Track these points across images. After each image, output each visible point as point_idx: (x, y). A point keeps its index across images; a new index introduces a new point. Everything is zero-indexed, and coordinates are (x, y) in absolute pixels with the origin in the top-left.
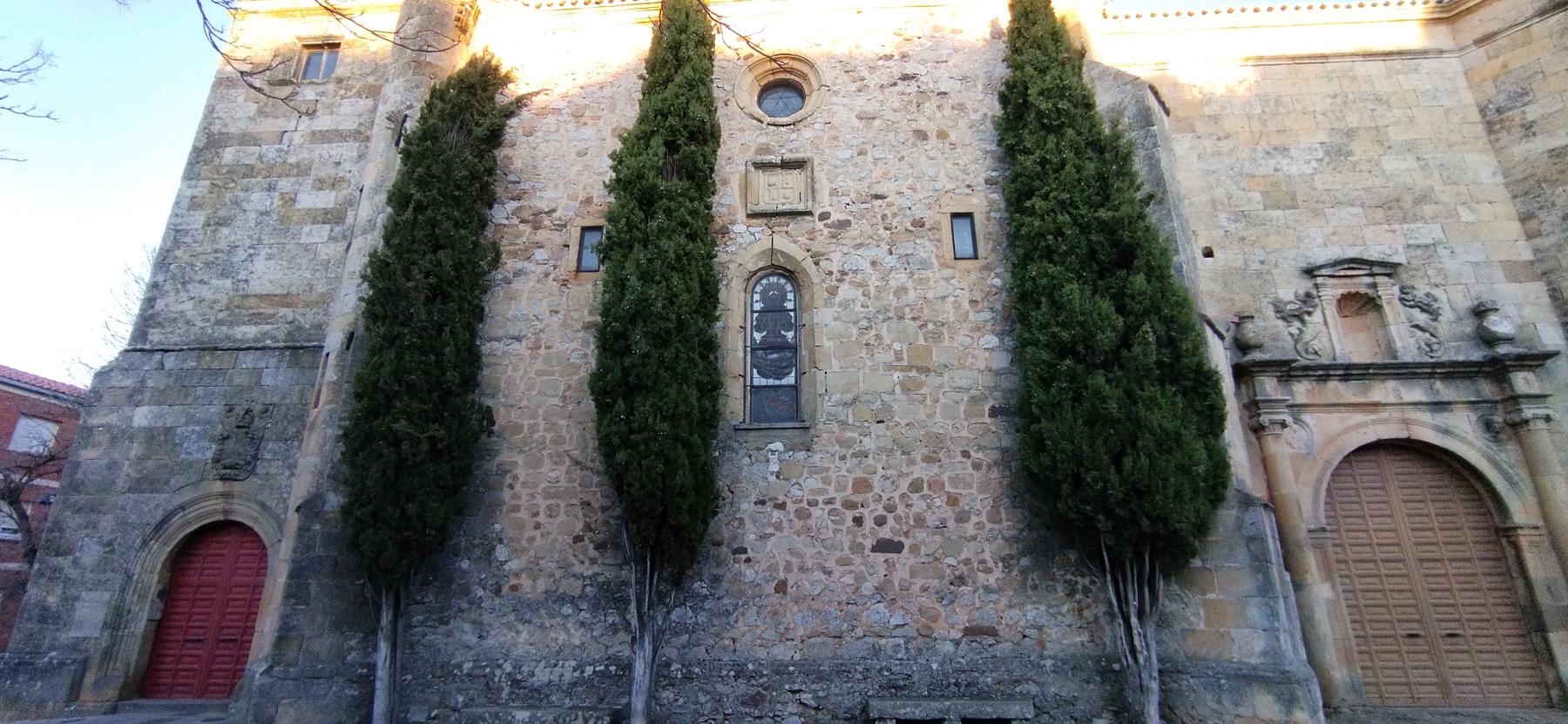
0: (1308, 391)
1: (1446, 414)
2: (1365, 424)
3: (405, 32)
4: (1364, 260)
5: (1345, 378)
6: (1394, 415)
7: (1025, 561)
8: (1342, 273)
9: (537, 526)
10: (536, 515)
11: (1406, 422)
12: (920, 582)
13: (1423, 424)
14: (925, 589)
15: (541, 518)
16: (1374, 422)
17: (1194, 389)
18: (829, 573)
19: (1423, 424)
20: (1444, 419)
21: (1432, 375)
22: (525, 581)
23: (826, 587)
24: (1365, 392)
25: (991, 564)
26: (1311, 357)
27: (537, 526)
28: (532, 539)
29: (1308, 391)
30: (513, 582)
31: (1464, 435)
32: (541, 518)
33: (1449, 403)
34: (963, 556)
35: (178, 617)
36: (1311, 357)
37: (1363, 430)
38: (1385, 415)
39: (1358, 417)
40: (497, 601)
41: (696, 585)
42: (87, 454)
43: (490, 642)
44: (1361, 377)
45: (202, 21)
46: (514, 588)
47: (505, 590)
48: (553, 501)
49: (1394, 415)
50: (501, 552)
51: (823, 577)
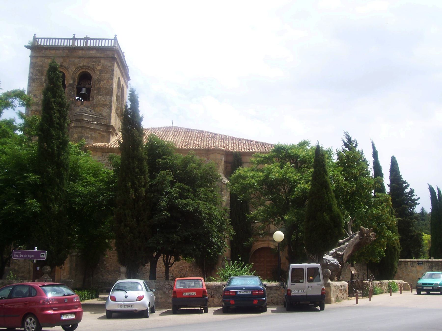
0: (110, 250)
4: (146, 288)
7: (193, 267)
9: (111, 258)
10: (111, 256)
12: (176, 270)
13: (272, 244)
14: (176, 271)
15: (112, 257)
16: (263, 243)
17: (362, 169)
18: (161, 268)
22: (110, 268)
23: (160, 270)
25: (187, 267)
27: (111, 258)
28: (110, 261)
29: (110, 250)
30: (107, 268)
32: (112, 257)
34: (183, 266)
40: (105, 271)
43: (104, 277)
46: (108, 269)
47: (106, 269)
48: (114, 254)
50: (105, 263)
51: (160, 268)
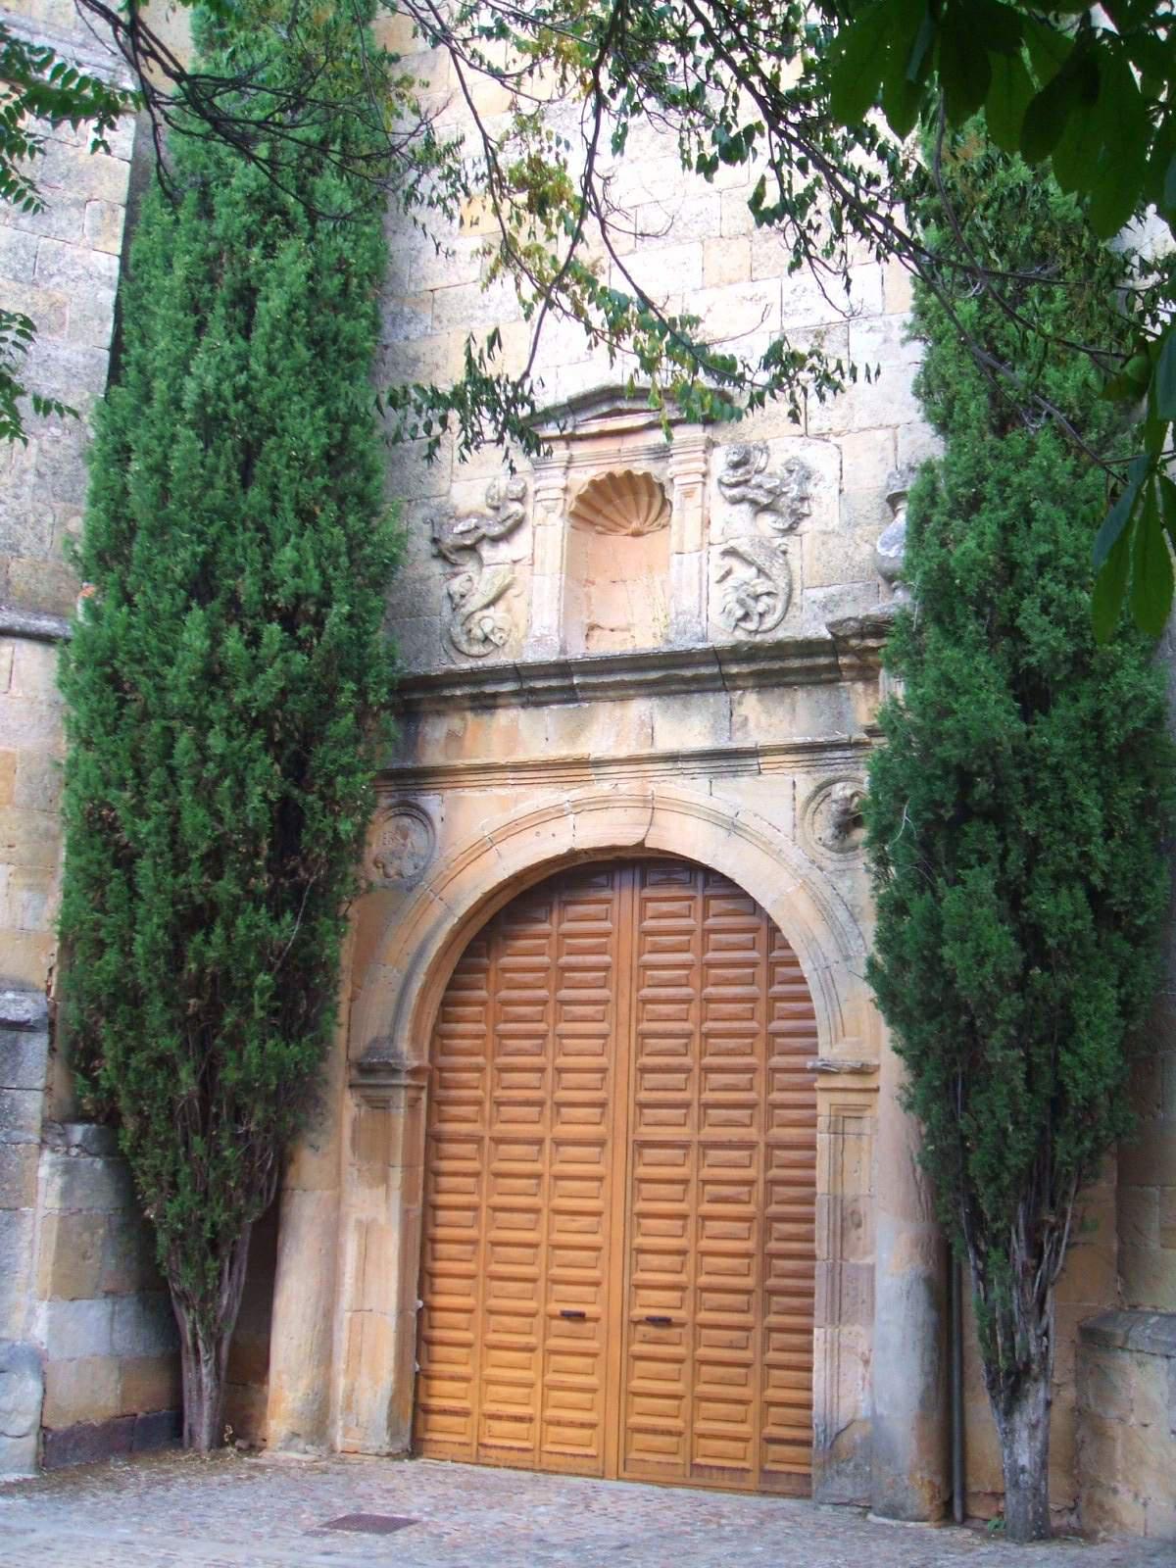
1: (745, 781)
2: (558, 813)
3: (171, 150)
5: (532, 699)
6: (623, 788)
8: (594, 427)
11: (649, 804)
13: (686, 808)
19: (686, 808)
20: (735, 794)
21: (724, 684)
24: (573, 736)
26: (476, 649)
31: (769, 832)
33: (754, 753)
35: (465, 1076)
36: (476, 649)
37: (553, 826)
38: (604, 788)
39: (543, 796)
41: (88, 1108)
42: (1041, 868)
44: (570, 695)
45: (851, 287)
49: (623, 788)
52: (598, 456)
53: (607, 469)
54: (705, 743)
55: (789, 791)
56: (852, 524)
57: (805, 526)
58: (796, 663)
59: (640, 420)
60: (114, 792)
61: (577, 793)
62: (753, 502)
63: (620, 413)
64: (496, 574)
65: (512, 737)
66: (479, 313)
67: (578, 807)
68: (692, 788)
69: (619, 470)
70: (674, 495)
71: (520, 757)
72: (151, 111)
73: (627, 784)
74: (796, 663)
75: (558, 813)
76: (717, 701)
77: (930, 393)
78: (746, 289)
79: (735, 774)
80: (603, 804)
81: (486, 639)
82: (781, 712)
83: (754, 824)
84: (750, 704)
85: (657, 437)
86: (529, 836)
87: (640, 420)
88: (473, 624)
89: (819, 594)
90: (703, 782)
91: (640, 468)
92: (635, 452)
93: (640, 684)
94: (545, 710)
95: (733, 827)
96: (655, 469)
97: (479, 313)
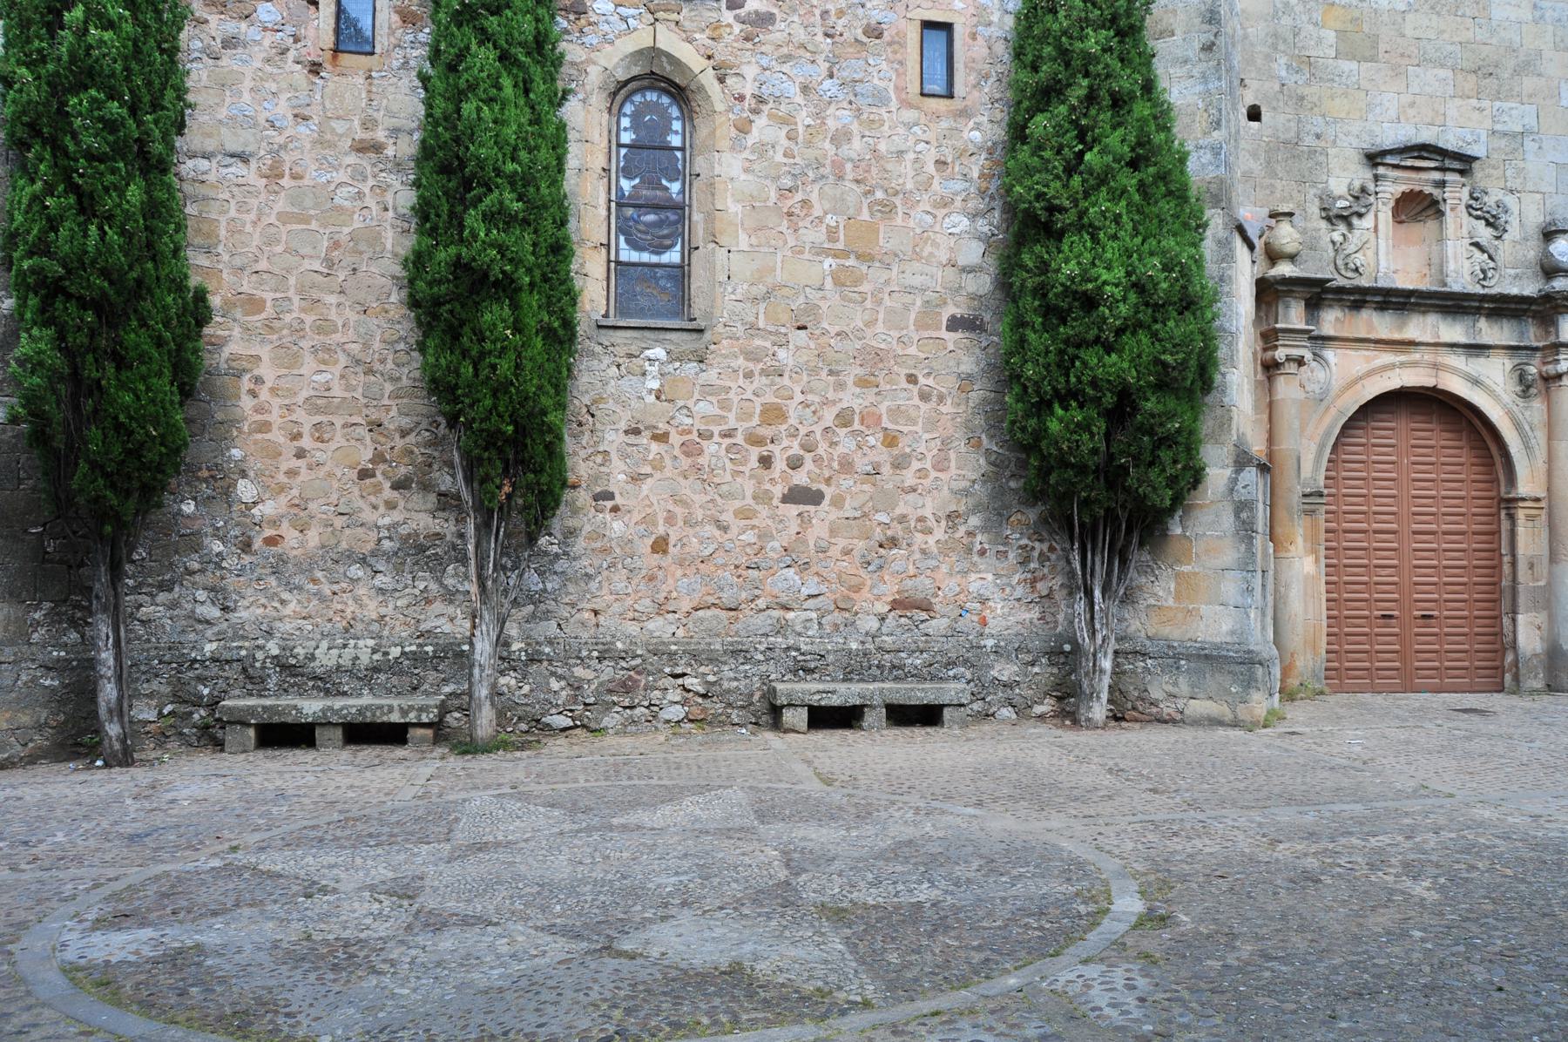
1: (1482, 360)
2: (1392, 366)
5: (1382, 307)
6: (1426, 357)
8: (1409, 163)
11: (1436, 366)
13: (1454, 371)
19: (1454, 371)
24: (1400, 328)
26: (1350, 274)
31: (1494, 387)
36: (1350, 274)
37: (1389, 373)
38: (1416, 356)
39: (1387, 358)
52: (1409, 179)
53: (1411, 187)
54: (1463, 340)
55: (1501, 367)
56: (1526, 239)
57: (1506, 236)
58: (1513, 306)
59: (1432, 164)
60: (751, 139)
61: (1403, 358)
62: (1487, 220)
63: (1425, 158)
64: (1362, 234)
65: (1371, 327)
66: (1337, 79)
67: (1402, 365)
68: (1457, 361)
69: (1417, 188)
70: (1447, 208)
71: (1372, 336)
72: (1110, 563)
73: (1427, 356)
74: (1513, 306)
75: (1392, 366)
76: (1468, 320)
77: (8, 624)
78: (1474, 102)
79: (1477, 356)
80: (1414, 364)
81: (1357, 270)
82: (1496, 328)
83: (1488, 382)
84: (1483, 323)
85: (1437, 176)
86: (1377, 378)
87: (1432, 164)
88: (1349, 260)
89: (1512, 272)
90: (1463, 358)
91: (1428, 189)
92: (1427, 181)
93: (1438, 306)
94: (1386, 313)
95: (1476, 382)
96: (1436, 192)
97: (1337, 79)
